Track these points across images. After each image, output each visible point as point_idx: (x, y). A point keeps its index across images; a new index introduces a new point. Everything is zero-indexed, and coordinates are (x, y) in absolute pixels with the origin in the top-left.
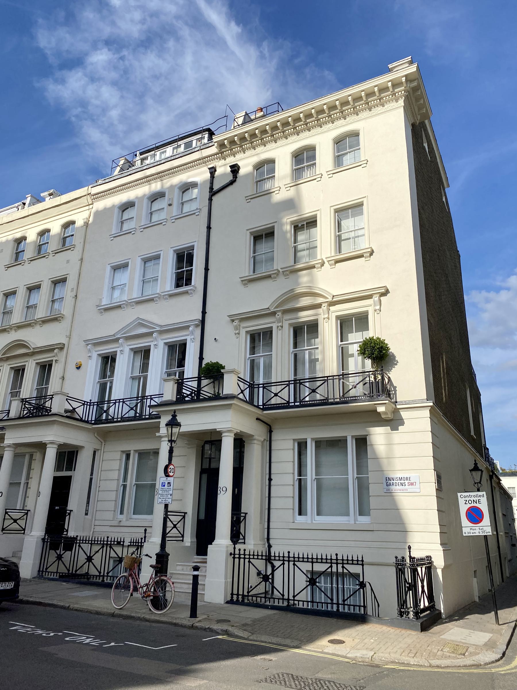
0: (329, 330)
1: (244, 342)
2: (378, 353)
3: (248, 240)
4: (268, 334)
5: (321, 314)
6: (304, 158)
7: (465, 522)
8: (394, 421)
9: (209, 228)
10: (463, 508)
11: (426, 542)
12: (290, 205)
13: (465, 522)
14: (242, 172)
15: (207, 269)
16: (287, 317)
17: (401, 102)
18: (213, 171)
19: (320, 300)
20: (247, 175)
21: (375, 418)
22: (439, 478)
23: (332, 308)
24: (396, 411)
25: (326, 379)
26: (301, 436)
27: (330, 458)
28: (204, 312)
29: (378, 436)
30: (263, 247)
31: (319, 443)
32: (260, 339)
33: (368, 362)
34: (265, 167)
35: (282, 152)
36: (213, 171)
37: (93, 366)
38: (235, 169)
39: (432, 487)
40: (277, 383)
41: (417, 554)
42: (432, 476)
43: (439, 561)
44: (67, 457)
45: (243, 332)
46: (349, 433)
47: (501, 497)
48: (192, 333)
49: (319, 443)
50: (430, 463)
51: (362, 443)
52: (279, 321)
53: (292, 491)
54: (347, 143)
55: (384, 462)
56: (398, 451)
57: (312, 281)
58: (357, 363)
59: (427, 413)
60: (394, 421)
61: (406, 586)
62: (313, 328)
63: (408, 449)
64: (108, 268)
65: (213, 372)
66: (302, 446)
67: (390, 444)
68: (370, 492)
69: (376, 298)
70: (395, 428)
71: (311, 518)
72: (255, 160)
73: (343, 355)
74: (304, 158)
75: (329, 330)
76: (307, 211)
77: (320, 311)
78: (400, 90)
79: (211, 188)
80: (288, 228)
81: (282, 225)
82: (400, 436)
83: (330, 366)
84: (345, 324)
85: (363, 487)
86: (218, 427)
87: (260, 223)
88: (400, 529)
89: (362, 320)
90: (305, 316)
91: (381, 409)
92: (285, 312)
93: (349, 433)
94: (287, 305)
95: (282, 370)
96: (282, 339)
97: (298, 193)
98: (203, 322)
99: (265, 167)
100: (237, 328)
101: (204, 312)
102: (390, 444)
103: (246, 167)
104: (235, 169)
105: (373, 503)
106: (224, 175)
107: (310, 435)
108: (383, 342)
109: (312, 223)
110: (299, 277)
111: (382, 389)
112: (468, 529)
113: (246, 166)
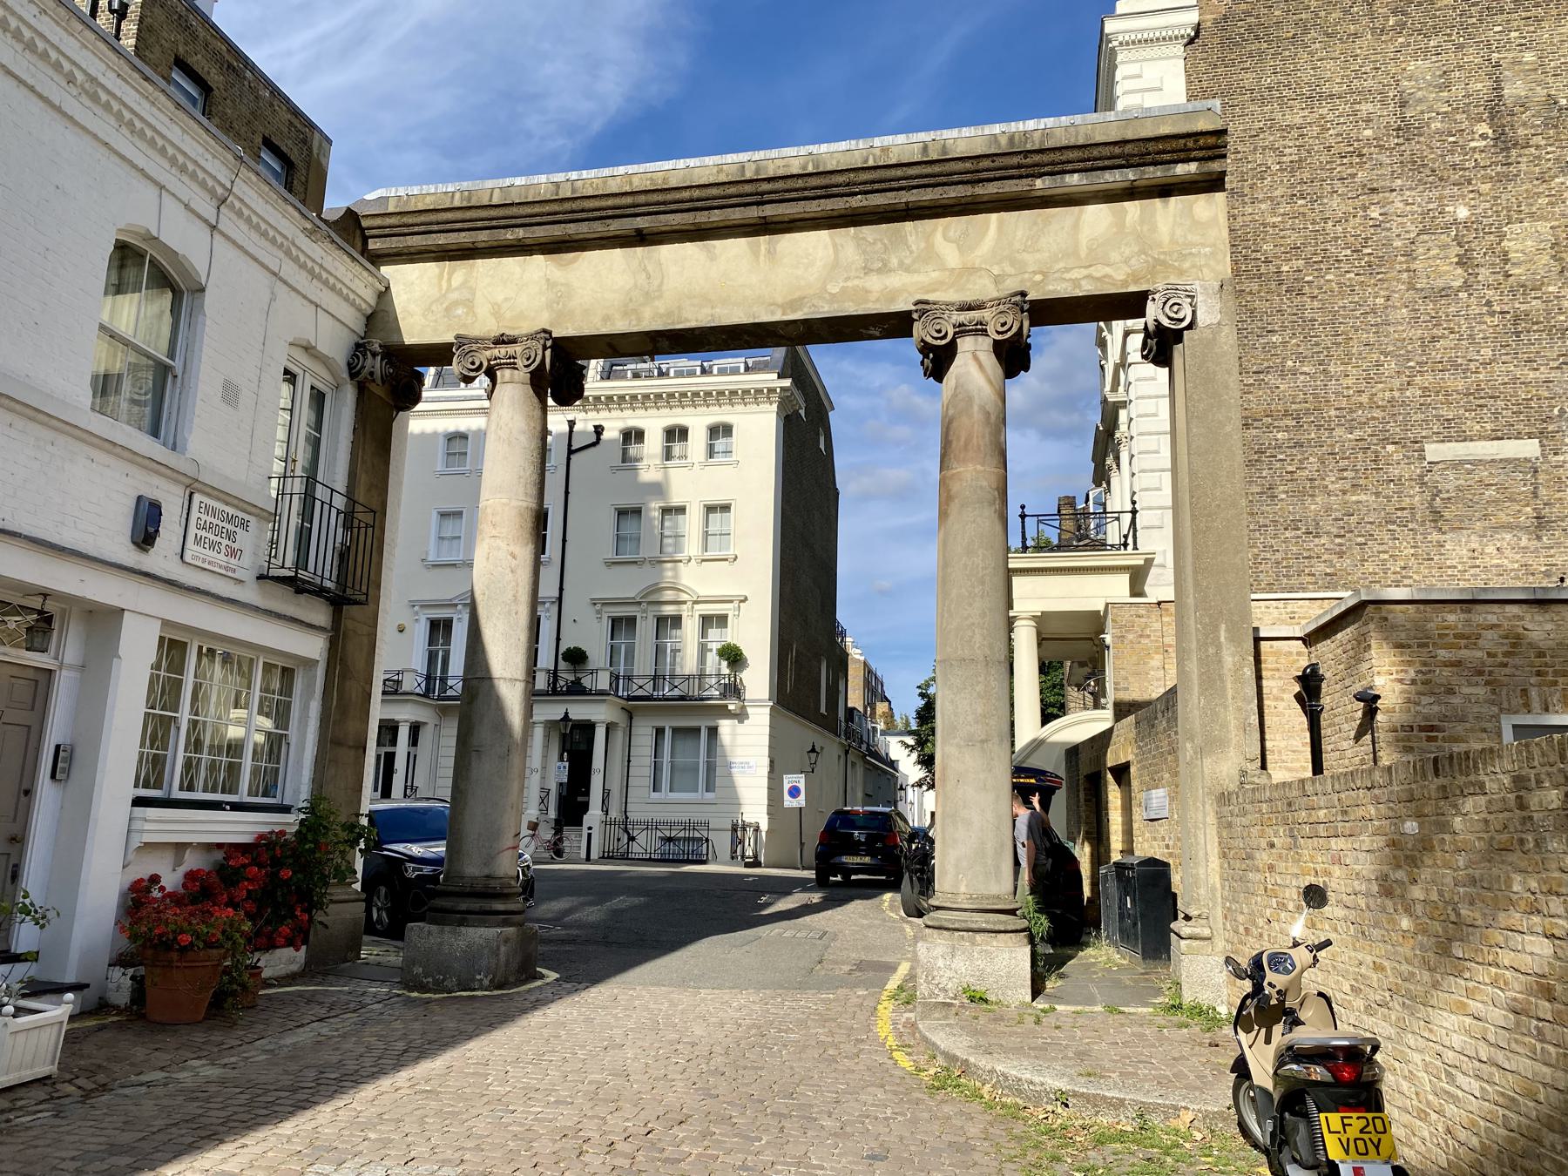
0: (691, 627)
1: (606, 625)
2: (734, 657)
3: (613, 515)
4: (631, 621)
5: (685, 611)
6: (676, 434)
7: (786, 796)
8: (741, 716)
9: (567, 493)
10: (786, 787)
11: (755, 810)
12: (658, 489)
13: (786, 796)
14: (606, 435)
15: (564, 541)
16: (651, 608)
17: (775, 406)
18: (572, 423)
19: (684, 597)
20: (611, 441)
21: (724, 712)
22: (772, 762)
23: (697, 607)
24: (744, 707)
25: (688, 678)
26: (659, 724)
27: (685, 745)
28: (561, 589)
29: (726, 727)
30: (629, 526)
31: (675, 730)
32: (622, 625)
33: (724, 664)
34: (633, 436)
35: (654, 424)
36: (572, 423)
37: (421, 631)
38: (599, 430)
39: (765, 770)
40: (639, 677)
41: (748, 818)
42: (766, 761)
43: (764, 827)
44: (415, 729)
45: (605, 617)
46: (704, 724)
47: (865, 776)
48: (548, 610)
49: (675, 730)
50: (766, 751)
51: (713, 732)
52: (645, 611)
53: (648, 771)
54: (720, 431)
55: (728, 749)
56: (740, 740)
57: (676, 576)
58: (713, 662)
59: (768, 710)
60: (741, 716)
61: (737, 842)
62: (677, 621)
63: (748, 741)
64: (435, 515)
65: (576, 657)
66: (660, 732)
67: (734, 735)
68: (714, 773)
69: (736, 604)
70: (741, 722)
71: (665, 794)
72: (621, 425)
73: (703, 650)
74: (676, 434)
75: (691, 627)
76: (675, 501)
77: (684, 607)
78: (775, 397)
79: (570, 445)
80: (656, 514)
81: (649, 510)
82: (742, 728)
83: (689, 665)
84: (707, 621)
85: (711, 768)
86: (593, 718)
87: (627, 502)
88: (734, 802)
89: (722, 620)
90: (669, 610)
91: (731, 707)
92: (649, 603)
93: (704, 724)
94: (651, 596)
95: (643, 665)
96: (646, 628)
97: (666, 475)
98: (560, 599)
99: (633, 436)
100: (598, 612)
101: (561, 589)
102: (734, 735)
103: (612, 433)
104: (599, 430)
105: (718, 781)
106: (584, 433)
107: (668, 724)
108: (738, 649)
109: (681, 510)
110: (662, 570)
111: (734, 690)
112: (789, 802)
113: (612, 429)
